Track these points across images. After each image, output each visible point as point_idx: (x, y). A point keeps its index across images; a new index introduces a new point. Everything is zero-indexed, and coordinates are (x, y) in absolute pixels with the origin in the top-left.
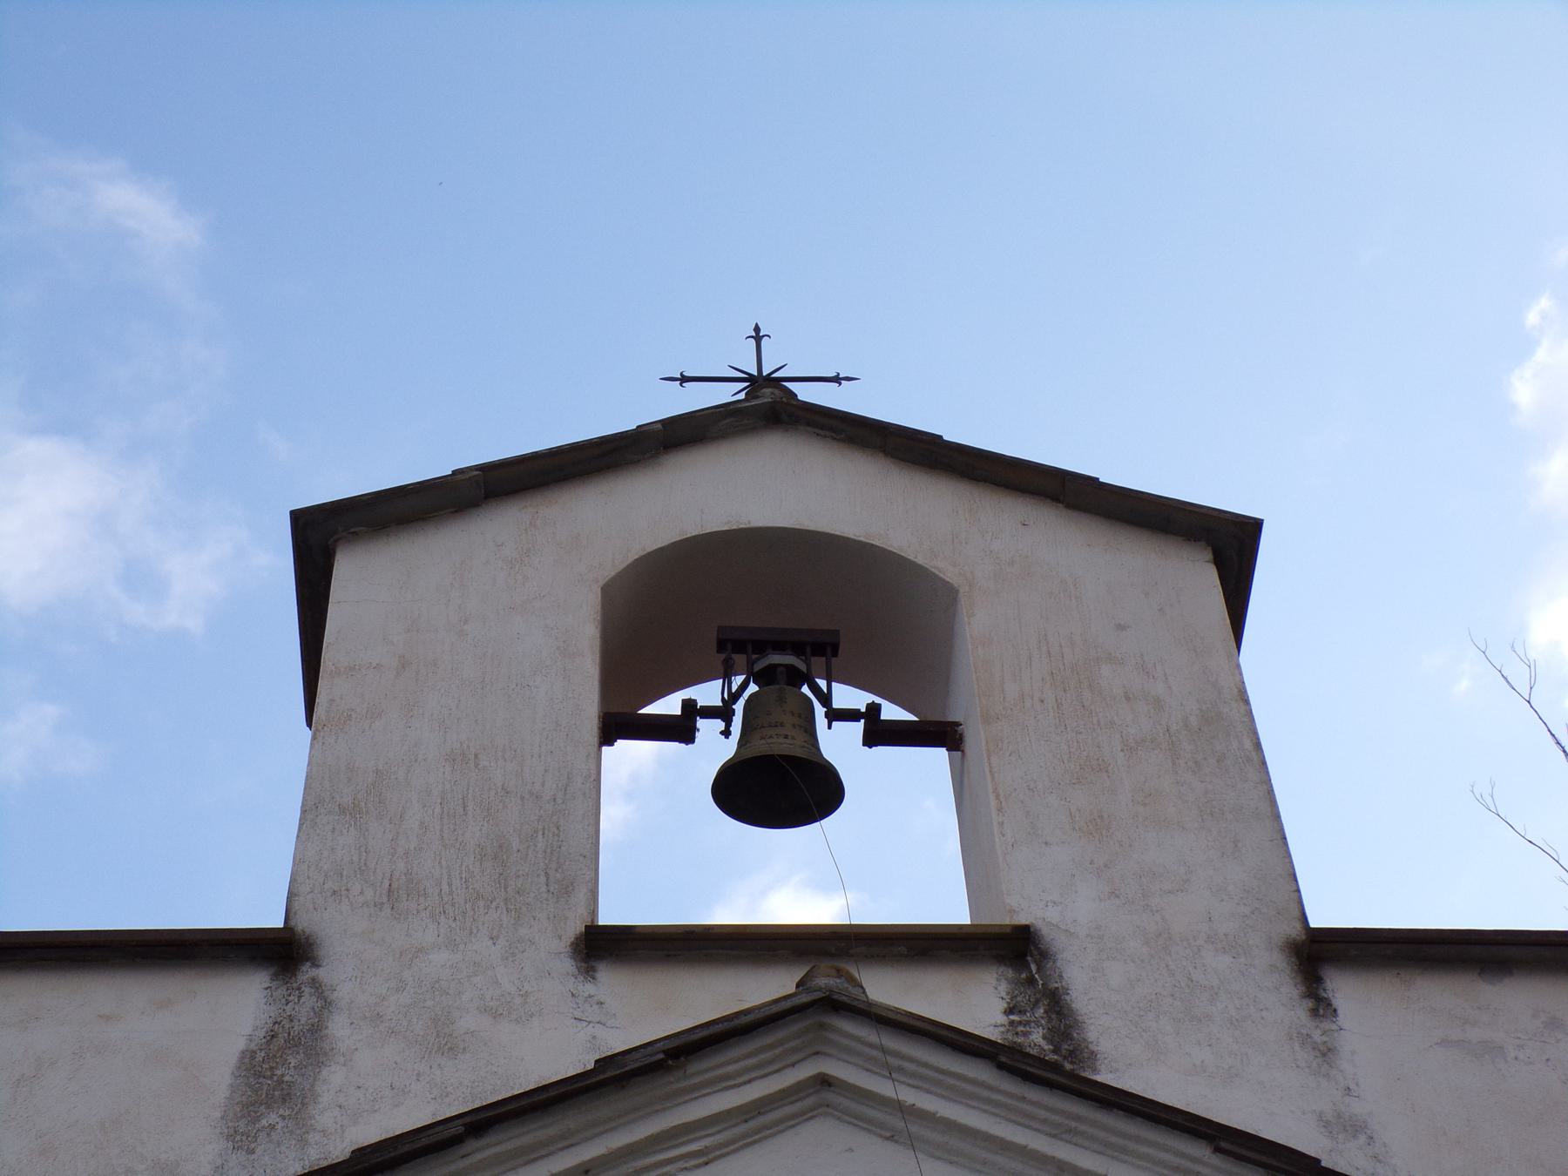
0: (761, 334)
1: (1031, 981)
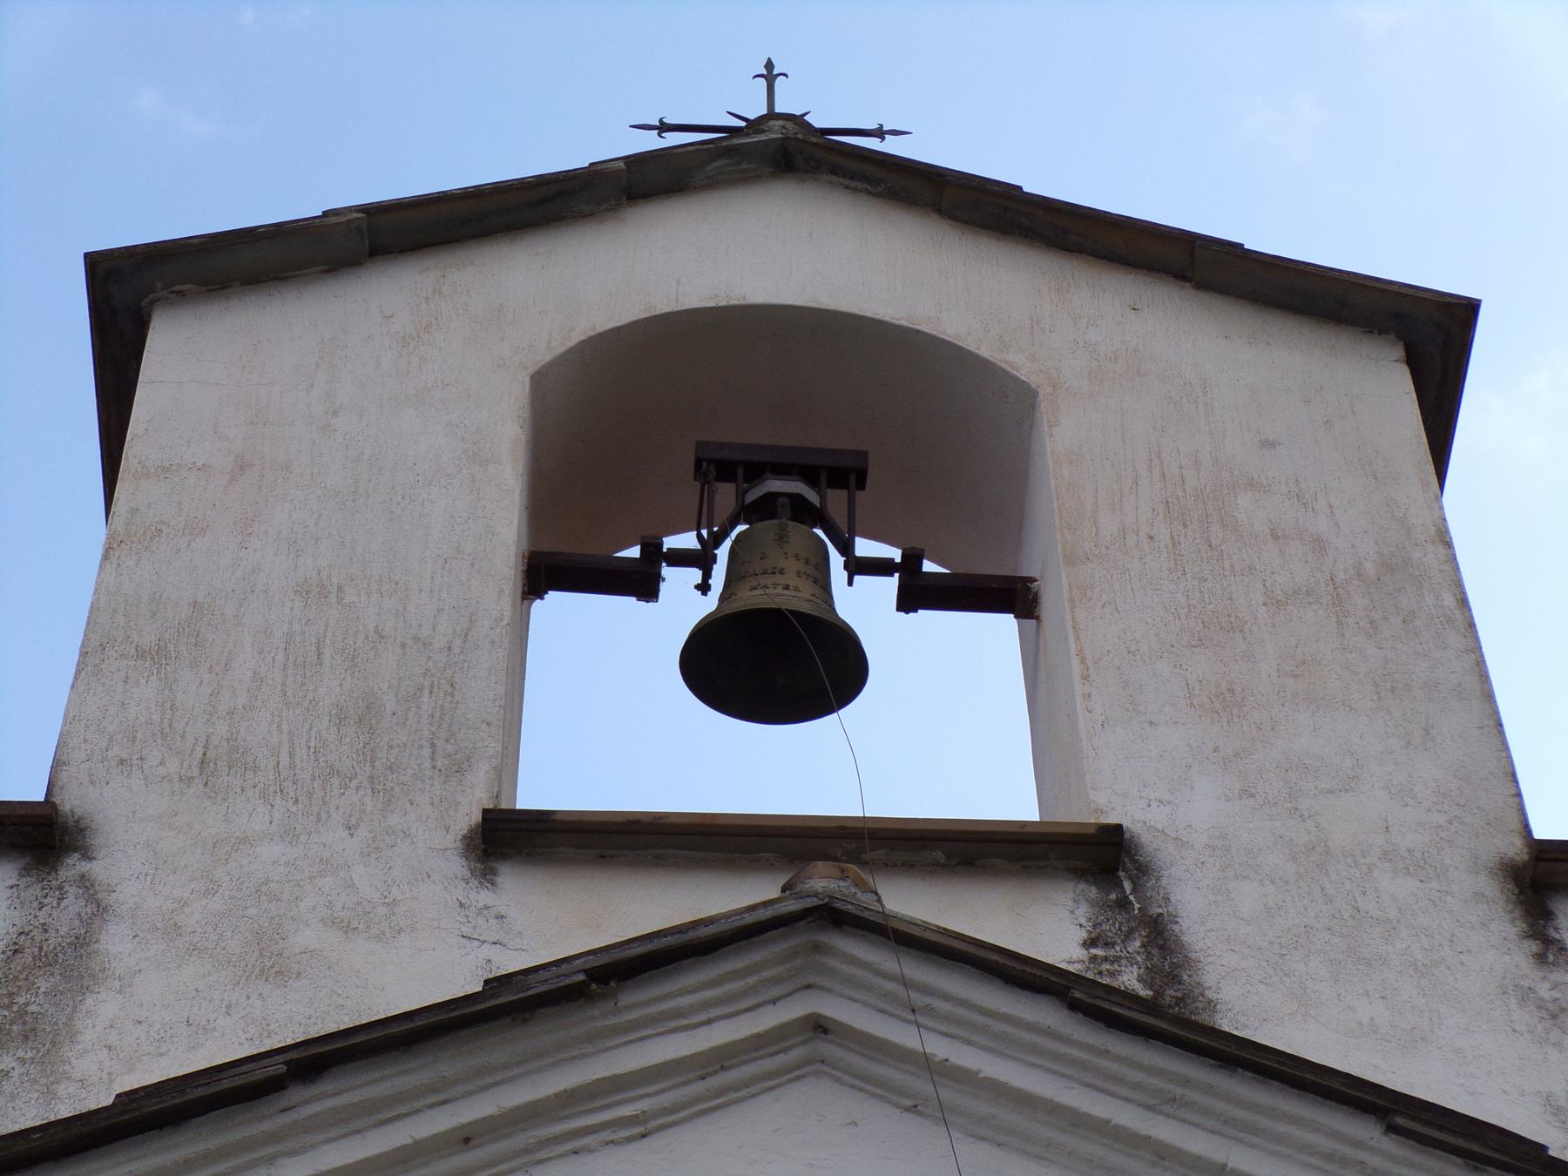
0: (775, 73)
1: (1123, 904)
